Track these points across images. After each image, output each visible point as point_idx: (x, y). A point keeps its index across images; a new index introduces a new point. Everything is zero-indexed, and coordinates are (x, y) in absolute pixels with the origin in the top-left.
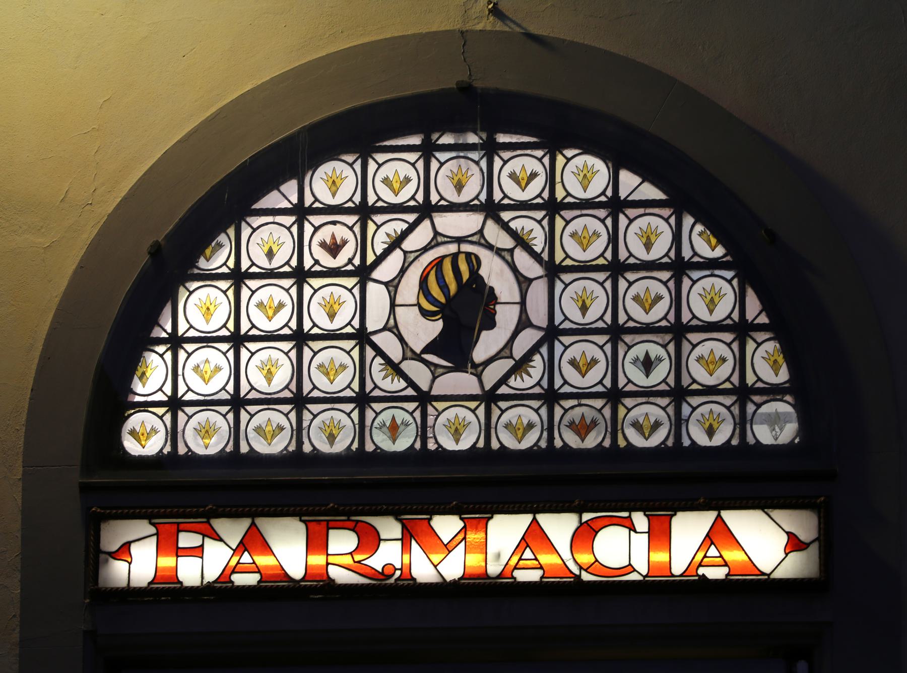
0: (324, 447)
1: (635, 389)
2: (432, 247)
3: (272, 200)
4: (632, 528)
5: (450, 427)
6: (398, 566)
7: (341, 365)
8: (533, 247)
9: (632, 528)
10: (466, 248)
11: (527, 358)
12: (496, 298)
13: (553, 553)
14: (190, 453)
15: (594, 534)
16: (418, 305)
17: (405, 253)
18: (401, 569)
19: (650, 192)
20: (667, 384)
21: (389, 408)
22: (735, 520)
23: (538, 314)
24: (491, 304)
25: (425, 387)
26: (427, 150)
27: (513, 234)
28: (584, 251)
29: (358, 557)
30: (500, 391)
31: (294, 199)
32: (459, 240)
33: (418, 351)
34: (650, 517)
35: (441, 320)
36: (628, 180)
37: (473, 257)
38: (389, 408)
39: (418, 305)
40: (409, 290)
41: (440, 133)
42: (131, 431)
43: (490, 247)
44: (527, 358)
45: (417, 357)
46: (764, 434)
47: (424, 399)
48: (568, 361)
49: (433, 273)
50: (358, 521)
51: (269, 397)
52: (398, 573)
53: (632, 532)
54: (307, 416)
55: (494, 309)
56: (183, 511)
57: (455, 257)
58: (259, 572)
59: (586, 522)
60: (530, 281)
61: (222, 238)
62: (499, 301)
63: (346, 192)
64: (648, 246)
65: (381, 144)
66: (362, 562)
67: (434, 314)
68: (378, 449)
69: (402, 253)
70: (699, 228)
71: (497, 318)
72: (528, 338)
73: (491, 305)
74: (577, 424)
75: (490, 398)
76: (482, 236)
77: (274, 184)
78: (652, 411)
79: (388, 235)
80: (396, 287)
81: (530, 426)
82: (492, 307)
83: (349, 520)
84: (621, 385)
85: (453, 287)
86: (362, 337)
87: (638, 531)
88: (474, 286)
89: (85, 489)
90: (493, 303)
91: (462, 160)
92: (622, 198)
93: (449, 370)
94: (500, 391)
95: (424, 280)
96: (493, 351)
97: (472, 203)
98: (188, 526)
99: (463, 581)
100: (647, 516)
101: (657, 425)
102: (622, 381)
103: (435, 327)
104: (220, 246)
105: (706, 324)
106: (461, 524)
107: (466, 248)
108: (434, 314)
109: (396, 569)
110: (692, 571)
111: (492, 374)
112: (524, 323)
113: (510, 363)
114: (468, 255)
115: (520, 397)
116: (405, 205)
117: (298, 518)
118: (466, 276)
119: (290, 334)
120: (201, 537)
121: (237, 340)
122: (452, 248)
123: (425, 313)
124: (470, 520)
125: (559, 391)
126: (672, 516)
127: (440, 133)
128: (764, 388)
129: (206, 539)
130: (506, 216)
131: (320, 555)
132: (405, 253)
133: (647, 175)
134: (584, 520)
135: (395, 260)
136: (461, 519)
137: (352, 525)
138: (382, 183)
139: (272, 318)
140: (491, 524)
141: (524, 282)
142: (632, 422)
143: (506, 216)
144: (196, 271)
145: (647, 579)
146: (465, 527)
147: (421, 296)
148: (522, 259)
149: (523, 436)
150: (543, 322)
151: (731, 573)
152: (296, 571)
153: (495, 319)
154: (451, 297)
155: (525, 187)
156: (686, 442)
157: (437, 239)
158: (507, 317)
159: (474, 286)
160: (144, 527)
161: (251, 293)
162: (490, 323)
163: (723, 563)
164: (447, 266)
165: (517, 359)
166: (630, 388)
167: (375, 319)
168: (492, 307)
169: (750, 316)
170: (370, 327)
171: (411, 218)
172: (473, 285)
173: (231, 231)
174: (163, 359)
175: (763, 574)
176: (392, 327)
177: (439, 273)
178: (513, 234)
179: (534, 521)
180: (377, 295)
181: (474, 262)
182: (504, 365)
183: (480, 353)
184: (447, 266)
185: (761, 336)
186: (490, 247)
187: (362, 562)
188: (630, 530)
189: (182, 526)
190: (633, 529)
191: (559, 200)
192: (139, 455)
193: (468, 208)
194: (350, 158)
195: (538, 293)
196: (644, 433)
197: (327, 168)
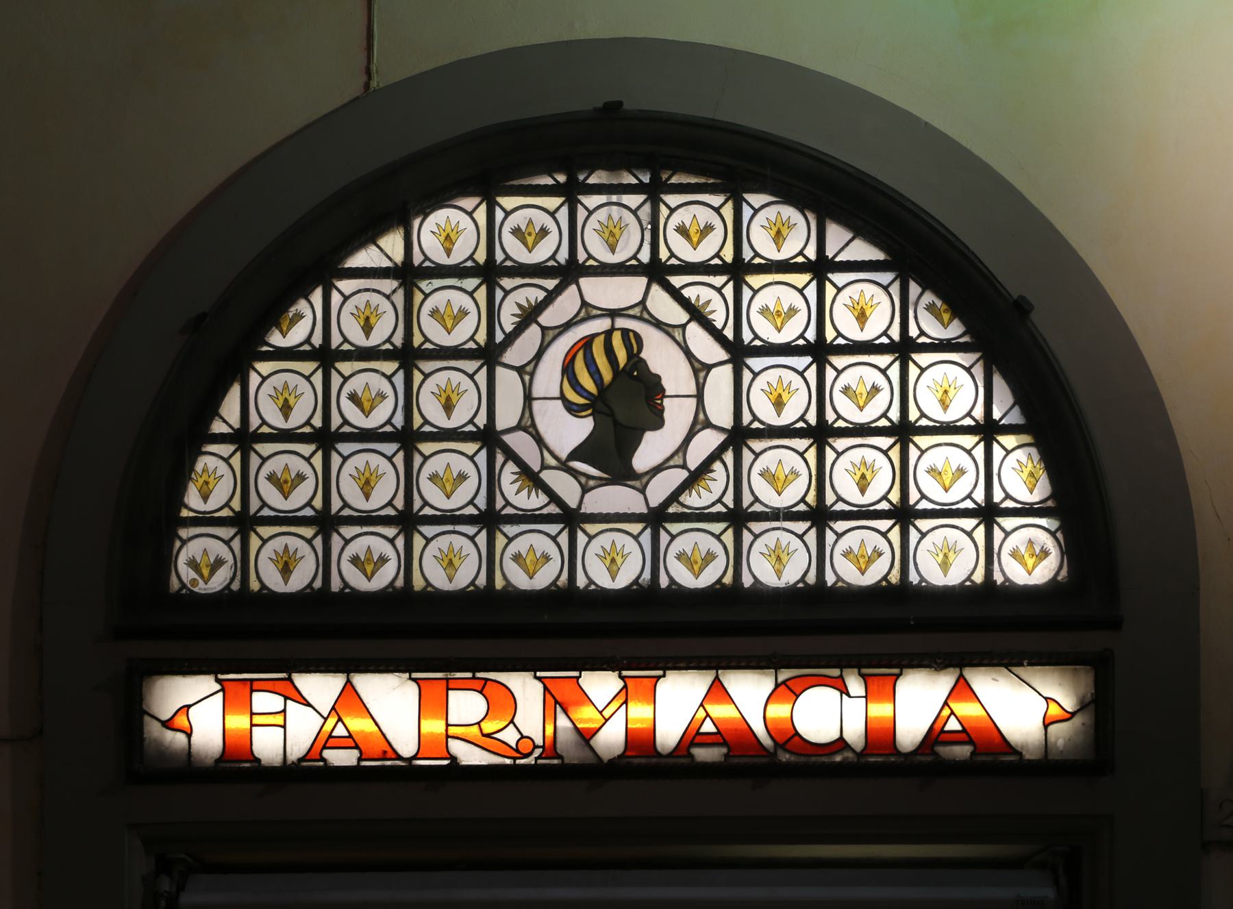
0: (604, 581)
1: (930, 506)
2: (577, 323)
3: (365, 258)
4: (844, 691)
5: (442, 560)
6: (539, 741)
7: (958, 469)
8: (714, 322)
9: (844, 691)
10: (621, 323)
11: (705, 467)
12: (663, 390)
13: (963, 717)
14: (184, 591)
15: (795, 697)
16: (562, 397)
17: (683, 327)
18: (543, 747)
19: (862, 251)
20: (476, 506)
21: (607, 530)
22: (369, 685)
23: (720, 411)
24: (657, 397)
25: (573, 504)
26: (571, 193)
27: (685, 303)
28: (779, 331)
29: (489, 727)
30: (671, 510)
31: (399, 257)
32: (613, 314)
33: (564, 455)
34: (421, 683)
35: (591, 418)
36: (836, 235)
37: (631, 335)
38: (607, 530)
39: (562, 397)
40: (548, 378)
41: (670, 172)
42: (515, 556)
43: (658, 324)
44: (705, 467)
45: (564, 466)
46: (845, 572)
47: (572, 519)
48: (267, 476)
49: (580, 355)
50: (487, 680)
51: (946, 508)
52: (538, 752)
53: (844, 696)
54: (255, 542)
55: (661, 404)
56: (691, 663)
57: (608, 334)
58: (357, 747)
59: (784, 683)
60: (708, 368)
61: (302, 306)
62: (667, 393)
63: (468, 246)
64: (367, 329)
65: (512, 183)
66: (495, 736)
67: (583, 407)
68: (264, 590)
69: (539, 329)
70: (929, 298)
71: (666, 415)
72: (707, 442)
73: (658, 399)
74: (363, 560)
75: (656, 518)
76: (645, 308)
77: (369, 235)
78: (375, 543)
79: (709, 302)
80: (532, 374)
81: (219, 563)
82: (659, 402)
83: (474, 678)
84: (745, 504)
85: (607, 375)
86: (489, 437)
87: (852, 695)
88: (635, 374)
89: (1115, 624)
90: (660, 396)
91: (615, 208)
92: (416, 265)
93: (607, 482)
94: (671, 510)
95: (568, 363)
96: (657, 459)
97: (628, 264)
98: (269, 685)
99: (305, 764)
100: (863, 676)
101: (710, 557)
102: (254, 504)
103: (582, 428)
104: (299, 317)
105: (357, 431)
106: (621, 684)
107: (621, 323)
108: (583, 407)
109: (536, 747)
110: (314, 754)
111: (659, 490)
112: (700, 423)
113: (681, 475)
114: (625, 332)
115: (701, 516)
116: (792, 261)
117: (856, 670)
118: (622, 356)
119: (391, 432)
120: (282, 699)
121: (903, 431)
122: (602, 324)
123: (572, 408)
124: (428, 683)
125: (917, 507)
126: (898, 676)
127: (670, 172)
128: (516, 515)
129: (289, 702)
130: (677, 281)
131: (730, 717)
132: (683, 327)
133: (860, 231)
134: (780, 679)
135: (531, 337)
136: (622, 677)
137: (479, 685)
138: (675, 232)
139: (863, 407)
140: (662, 686)
141: (701, 370)
142: (350, 557)
143: (677, 281)
144: (265, 348)
145: (863, 760)
146: (625, 687)
147: (566, 384)
148: (698, 338)
149: (701, 570)
150: (726, 421)
151: (363, 757)
152: (406, 746)
153: (663, 416)
154: (605, 387)
155: (534, 247)
156: (254, 585)
157: (587, 311)
158: (678, 414)
159: (635, 374)
160: (205, 684)
161: (342, 380)
162: (657, 422)
163: (353, 745)
164: (598, 348)
165: (692, 469)
166: (924, 505)
167: (507, 415)
168: (659, 402)
169: (996, 415)
170: (501, 425)
171: (551, 284)
172: (634, 372)
173: (317, 296)
174: (311, 464)
175: (399, 757)
176: (528, 425)
177: (589, 355)
178: (685, 303)
179: (717, 681)
180: (508, 383)
181: (633, 342)
182: (676, 477)
183: (642, 460)
184: (598, 348)
185: (1009, 441)
186: (658, 324)
187: (495, 736)
188: (842, 693)
189: (256, 685)
190: (846, 691)
191: (498, 263)
192: (826, 581)
193: (622, 270)
194: (468, 203)
195: (720, 381)
196: (365, 570)
197: (440, 217)
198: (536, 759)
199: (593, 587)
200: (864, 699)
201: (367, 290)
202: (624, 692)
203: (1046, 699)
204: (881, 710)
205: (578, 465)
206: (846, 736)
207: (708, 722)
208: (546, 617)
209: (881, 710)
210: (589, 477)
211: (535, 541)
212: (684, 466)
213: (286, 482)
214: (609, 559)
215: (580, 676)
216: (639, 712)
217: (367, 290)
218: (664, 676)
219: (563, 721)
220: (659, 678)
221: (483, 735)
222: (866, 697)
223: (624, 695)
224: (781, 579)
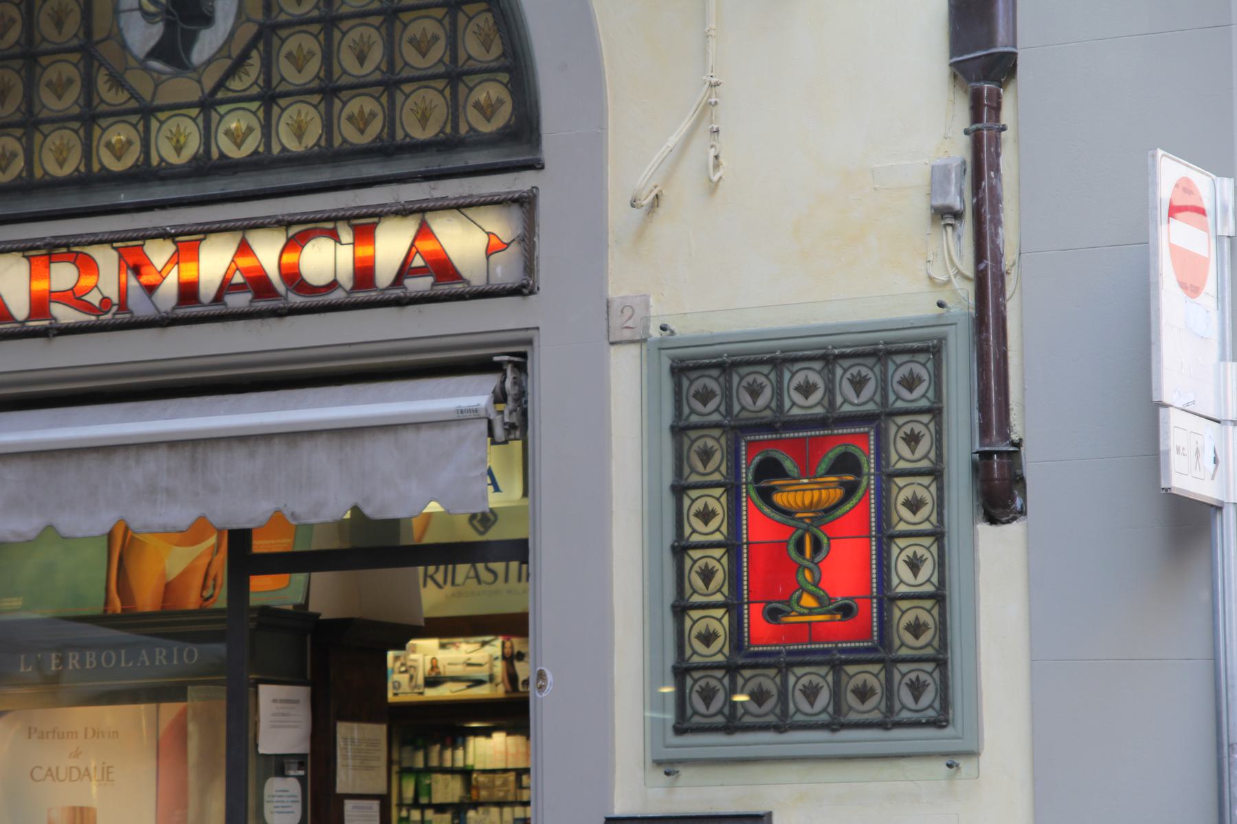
16: (141, 8)
39: (141, 8)
67: (154, 15)
175: (17, 322)
198: (114, 314)
199: (408, 140)
200: (351, 246)
201: (915, 524)
202: (176, 255)
203: (489, 234)
204: (364, 251)
205: (156, 65)
206: (339, 278)
207: (238, 273)
208: (122, 196)
209: (364, 251)
210: (160, 73)
211: (119, 134)
212: (229, 57)
213: (238, 136)
214: (175, 140)
215: (144, 245)
216: (188, 271)
217: (915, 524)
218: (204, 239)
219: (133, 282)
220: (201, 240)
221: (75, 298)
222: (354, 244)
223: (176, 259)
224: (166, 140)
